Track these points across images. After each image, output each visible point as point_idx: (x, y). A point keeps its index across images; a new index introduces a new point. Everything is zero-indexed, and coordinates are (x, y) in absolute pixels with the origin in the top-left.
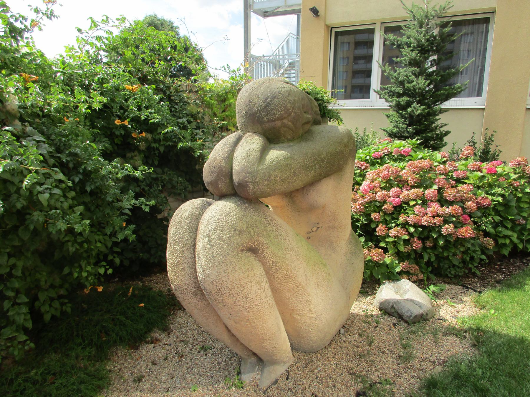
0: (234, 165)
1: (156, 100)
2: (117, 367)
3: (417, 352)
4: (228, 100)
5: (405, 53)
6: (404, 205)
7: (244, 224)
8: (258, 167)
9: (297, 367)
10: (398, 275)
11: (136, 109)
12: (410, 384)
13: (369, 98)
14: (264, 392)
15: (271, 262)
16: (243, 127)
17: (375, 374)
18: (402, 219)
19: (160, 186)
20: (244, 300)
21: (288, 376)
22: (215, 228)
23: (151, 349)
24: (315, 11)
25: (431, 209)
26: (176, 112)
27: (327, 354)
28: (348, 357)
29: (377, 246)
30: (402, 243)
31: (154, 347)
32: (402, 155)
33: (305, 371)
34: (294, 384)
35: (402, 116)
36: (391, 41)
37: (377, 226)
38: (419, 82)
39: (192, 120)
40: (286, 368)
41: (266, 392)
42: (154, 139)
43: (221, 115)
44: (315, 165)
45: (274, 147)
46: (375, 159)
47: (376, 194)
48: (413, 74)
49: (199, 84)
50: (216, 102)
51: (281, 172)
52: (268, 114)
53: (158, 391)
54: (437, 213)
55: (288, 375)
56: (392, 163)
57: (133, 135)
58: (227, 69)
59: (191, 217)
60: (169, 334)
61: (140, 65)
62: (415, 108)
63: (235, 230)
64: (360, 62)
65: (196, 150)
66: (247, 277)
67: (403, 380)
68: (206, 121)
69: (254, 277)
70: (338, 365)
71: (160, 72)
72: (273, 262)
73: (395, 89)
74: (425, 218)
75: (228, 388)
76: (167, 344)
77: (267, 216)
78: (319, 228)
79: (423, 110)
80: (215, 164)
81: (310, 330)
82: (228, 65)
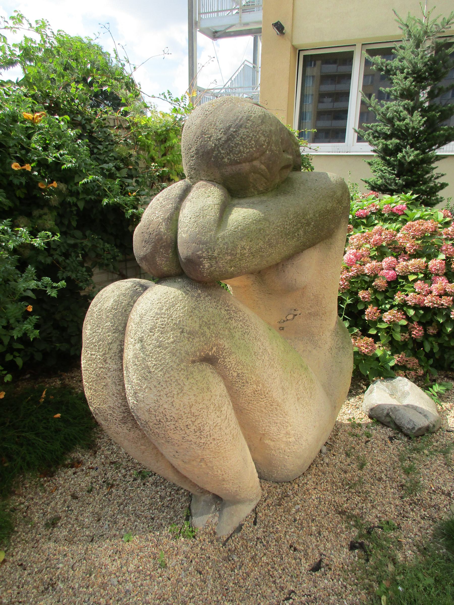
0: (179, 231)
1: (71, 136)
2: (23, 503)
3: (424, 479)
4: (169, 141)
5: (396, 81)
6: (400, 280)
7: (195, 322)
8: (216, 233)
9: (268, 505)
10: (392, 372)
11: (41, 148)
12: (421, 528)
13: (344, 142)
14: (224, 544)
15: (235, 374)
16: (192, 173)
17: (372, 513)
18: (399, 299)
19: (80, 255)
20: (197, 434)
21: (256, 519)
22: (151, 329)
23: (71, 475)
24: (279, 27)
25: (437, 285)
26: (100, 154)
27: (306, 483)
28: (334, 487)
29: (365, 333)
30: (399, 330)
31: (74, 473)
32: (393, 214)
33: (278, 512)
34: (264, 532)
35: (389, 164)
36: (377, 64)
37: (366, 308)
38: (414, 119)
39: (122, 165)
40: (252, 506)
41: (227, 544)
42: (70, 191)
43: (160, 159)
44: (298, 229)
45: (238, 204)
46: (360, 218)
47: (364, 265)
48: (405, 108)
49: (131, 118)
50: (153, 143)
51: (251, 241)
52: (231, 151)
53: (79, 540)
54: (445, 291)
55: (256, 517)
56: (381, 223)
57: (40, 185)
58: (168, 97)
59: (116, 309)
60: (95, 453)
61: (48, 89)
62: (407, 153)
63: (182, 332)
64: (326, 100)
65: (128, 208)
66: (201, 401)
67: (410, 522)
68: (141, 168)
69: (212, 400)
70: (321, 500)
71: (77, 99)
72: (238, 374)
73: (382, 129)
74: (429, 297)
75: (174, 538)
76: (92, 468)
77: (229, 306)
78: (296, 315)
79: (417, 155)
80: (151, 230)
81: (287, 457)
82: (169, 92)
